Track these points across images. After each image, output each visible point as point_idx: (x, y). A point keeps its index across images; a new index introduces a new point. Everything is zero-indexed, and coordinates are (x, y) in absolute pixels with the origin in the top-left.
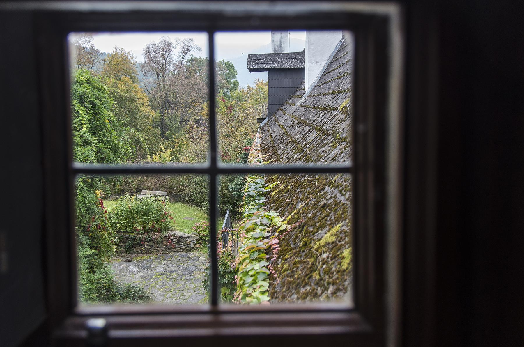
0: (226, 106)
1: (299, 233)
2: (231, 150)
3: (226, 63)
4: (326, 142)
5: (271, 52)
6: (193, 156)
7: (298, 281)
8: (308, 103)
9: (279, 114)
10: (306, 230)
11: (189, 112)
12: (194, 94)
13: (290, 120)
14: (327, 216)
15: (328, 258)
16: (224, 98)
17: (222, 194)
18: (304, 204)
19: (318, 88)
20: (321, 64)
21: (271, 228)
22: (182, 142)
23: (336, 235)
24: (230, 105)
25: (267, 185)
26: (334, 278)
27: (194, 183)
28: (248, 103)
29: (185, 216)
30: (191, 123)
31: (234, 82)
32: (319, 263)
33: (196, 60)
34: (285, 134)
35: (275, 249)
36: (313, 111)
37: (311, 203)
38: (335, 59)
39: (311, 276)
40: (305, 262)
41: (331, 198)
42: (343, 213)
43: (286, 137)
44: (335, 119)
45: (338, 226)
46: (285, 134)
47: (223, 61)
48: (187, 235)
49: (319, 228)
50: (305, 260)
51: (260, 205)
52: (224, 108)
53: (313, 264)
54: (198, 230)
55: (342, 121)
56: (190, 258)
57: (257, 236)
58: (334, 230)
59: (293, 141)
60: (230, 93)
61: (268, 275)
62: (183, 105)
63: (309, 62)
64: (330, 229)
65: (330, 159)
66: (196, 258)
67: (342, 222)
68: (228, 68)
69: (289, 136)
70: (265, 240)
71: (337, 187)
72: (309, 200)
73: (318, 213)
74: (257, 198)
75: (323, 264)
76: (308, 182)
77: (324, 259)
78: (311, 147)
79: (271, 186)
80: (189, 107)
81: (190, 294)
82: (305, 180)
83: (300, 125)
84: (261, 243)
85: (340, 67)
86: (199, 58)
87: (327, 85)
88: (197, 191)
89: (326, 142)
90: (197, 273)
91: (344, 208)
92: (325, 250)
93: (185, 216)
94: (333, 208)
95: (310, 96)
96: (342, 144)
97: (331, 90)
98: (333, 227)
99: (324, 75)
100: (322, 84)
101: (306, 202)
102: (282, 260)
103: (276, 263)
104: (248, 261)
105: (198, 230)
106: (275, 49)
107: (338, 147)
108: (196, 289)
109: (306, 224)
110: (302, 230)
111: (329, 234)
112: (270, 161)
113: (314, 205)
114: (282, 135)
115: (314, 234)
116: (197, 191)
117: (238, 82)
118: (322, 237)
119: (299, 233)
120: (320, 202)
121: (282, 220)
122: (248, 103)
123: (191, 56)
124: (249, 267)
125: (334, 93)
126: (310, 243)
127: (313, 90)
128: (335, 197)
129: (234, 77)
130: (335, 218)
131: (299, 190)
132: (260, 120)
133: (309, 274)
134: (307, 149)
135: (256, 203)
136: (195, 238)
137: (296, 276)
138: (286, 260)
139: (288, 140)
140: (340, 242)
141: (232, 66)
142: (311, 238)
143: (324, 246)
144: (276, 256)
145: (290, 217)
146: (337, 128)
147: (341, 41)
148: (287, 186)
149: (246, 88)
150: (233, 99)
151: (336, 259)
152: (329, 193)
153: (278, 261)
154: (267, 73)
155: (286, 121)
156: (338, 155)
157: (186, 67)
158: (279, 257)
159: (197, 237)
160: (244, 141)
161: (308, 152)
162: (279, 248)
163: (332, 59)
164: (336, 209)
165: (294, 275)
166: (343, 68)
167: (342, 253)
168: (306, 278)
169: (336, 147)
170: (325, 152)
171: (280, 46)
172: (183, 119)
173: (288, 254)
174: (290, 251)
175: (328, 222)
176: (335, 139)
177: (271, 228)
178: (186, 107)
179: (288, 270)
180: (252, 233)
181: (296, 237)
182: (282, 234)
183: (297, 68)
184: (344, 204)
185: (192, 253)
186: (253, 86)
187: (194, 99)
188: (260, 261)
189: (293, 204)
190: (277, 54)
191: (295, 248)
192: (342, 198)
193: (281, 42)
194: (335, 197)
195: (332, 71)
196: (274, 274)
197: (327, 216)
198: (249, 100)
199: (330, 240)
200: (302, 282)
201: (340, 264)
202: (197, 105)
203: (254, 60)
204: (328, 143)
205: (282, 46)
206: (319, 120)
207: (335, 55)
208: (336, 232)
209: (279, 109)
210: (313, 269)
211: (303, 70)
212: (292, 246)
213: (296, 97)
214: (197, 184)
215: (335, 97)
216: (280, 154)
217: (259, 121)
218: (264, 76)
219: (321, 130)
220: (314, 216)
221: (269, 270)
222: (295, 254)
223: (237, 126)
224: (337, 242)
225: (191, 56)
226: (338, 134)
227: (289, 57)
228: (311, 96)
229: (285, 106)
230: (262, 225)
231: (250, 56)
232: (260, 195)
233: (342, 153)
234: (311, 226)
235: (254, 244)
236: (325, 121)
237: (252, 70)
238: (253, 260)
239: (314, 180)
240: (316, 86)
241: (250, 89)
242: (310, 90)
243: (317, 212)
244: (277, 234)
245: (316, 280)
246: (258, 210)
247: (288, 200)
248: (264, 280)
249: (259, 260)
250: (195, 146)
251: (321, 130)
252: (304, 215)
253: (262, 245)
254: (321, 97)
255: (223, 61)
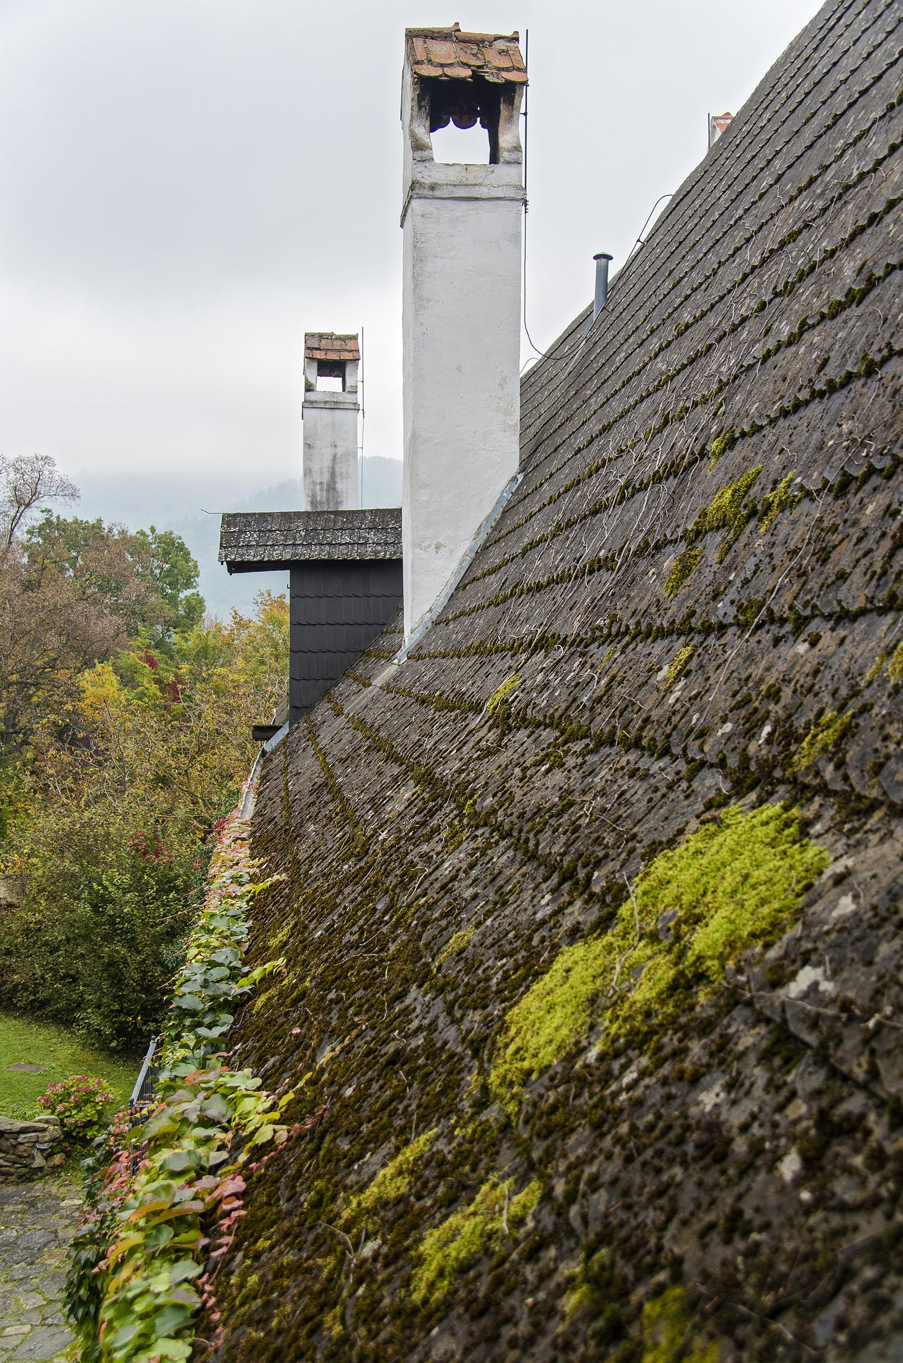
0: (158, 681)
1: (311, 1157)
2: (172, 829)
3: (160, 537)
4: (434, 822)
5: (303, 506)
6: (43, 851)
7: (279, 1341)
8: (405, 683)
9: (323, 711)
10: (329, 1150)
11: (35, 699)
12: (53, 640)
13: (348, 737)
14: (398, 1097)
15: (376, 1257)
16: (155, 653)
17: (143, 979)
18: (338, 1049)
19: (442, 630)
20: (452, 552)
21: (230, 1135)
22: (11, 803)
23: (412, 1172)
24: (172, 678)
25: (246, 969)
26: (383, 1335)
27: (46, 944)
28: (233, 673)
29: (16, 1059)
30: (42, 737)
31: (187, 599)
32: (347, 1277)
33: (61, 526)
34: (328, 787)
35: (227, 1214)
36: (416, 707)
37: (361, 1047)
38: (496, 535)
39: (318, 1326)
40: (308, 1270)
41: (420, 1028)
42: (443, 1092)
43: (327, 798)
44: (471, 744)
45: (423, 1138)
46: (328, 787)
47: (153, 530)
48: (20, 1124)
49: (368, 1142)
50: (311, 1262)
51: (214, 1046)
52: (154, 688)
53: (330, 1280)
54: (60, 1108)
55: (489, 753)
56: (32, 1204)
57: (178, 1167)
58: (409, 1154)
59: (347, 815)
60: (175, 638)
61: (196, 1314)
62: (14, 678)
63: (414, 545)
64: (398, 1149)
65: (437, 885)
66: (50, 1202)
67: (438, 1121)
68: (166, 553)
69: (337, 792)
70: (207, 1181)
71: (441, 990)
72: (354, 1033)
73: (375, 1086)
74: (207, 1020)
75: (359, 1282)
76: (363, 966)
77: (364, 1261)
78: (391, 840)
79: (257, 974)
80: (37, 685)
81: (27, 1328)
82: (355, 959)
83: (375, 756)
84: (189, 1193)
85: (505, 563)
86: (70, 520)
87: (467, 621)
88: (54, 971)
89: (434, 822)
90: (51, 1256)
91: (451, 1073)
92: (370, 1227)
93: (16, 1059)
94: (420, 1068)
95: (416, 655)
96: (479, 832)
97: (474, 640)
98: (407, 1142)
99: (461, 587)
100: (455, 618)
101: (347, 1042)
102: (245, 1257)
103: (224, 1268)
104: (139, 1258)
105: (60, 1108)
106: (314, 496)
107: (465, 844)
108: (48, 1311)
109: (333, 1124)
110: (318, 1149)
111: (389, 1170)
112: (269, 882)
113: (367, 1054)
114: (317, 790)
115: (349, 1165)
116: (54, 971)
117: (201, 601)
118: (372, 1178)
119: (311, 1157)
120: (385, 1042)
121: (268, 1105)
122: (233, 673)
123: (45, 515)
124: (137, 1284)
125: (479, 650)
126: (334, 1198)
127: (427, 636)
128: (432, 1027)
129: (188, 585)
130: (419, 1106)
131: (332, 995)
132: (263, 732)
133: (312, 1317)
134: (377, 847)
135: (199, 1039)
136: (47, 1136)
137: (274, 1323)
138: (257, 1257)
139: (331, 807)
140: (419, 1198)
141: (181, 547)
142: (336, 1178)
143: (371, 1212)
144: (229, 1239)
145: (290, 1096)
146: (472, 775)
147: (514, 479)
148: (302, 979)
149: (227, 621)
150: (185, 657)
151: (401, 1262)
152: (418, 1011)
153: (232, 1259)
154: (284, 576)
155: (337, 739)
156: (462, 875)
157: (26, 548)
158: (236, 1247)
159: (53, 1131)
160: (215, 799)
161: (379, 858)
162: (243, 1213)
163: (489, 535)
164: (428, 1075)
165: (270, 1317)
166: (512, 567)
167: (420, 1240)
168: (304, 1332)
169: (460, 843)
170: (426, 857)
171: (331, 487)
172: (14, 725)
173: (266, 1234)
174: (274, 1222)
175: (399, 1122)
176: (461, 816)
177: (230, 1135)
178: (23, 685)
179: (255, 1298)
180: (165, 1154)
181: (299, 1173)
182: (258, 1160)
183: (383, 561)
184: (452, 1055)
185: (39, 1185)
186: (251, 613)
187: (53, 655)
188: (177, 1260)
189: (307, 1047)
190: (320, 513)
191: (290, 1213)
192: (451, 1033)
193: (333, 475)
194: (432, 1027)
195: (484, 575)
196: (212, 1310)
197: (398, 1097)
198: (240, 662)
199: (391, 1192)
200: (290, 1346)
201: (407, 1282)
202: (61, 675)
203: (241, 532)
204: (437, 830)
205: (339, 486)
206: (429, 744)
207: (498, 524)
208: (416, 1160)
209: (326, 694)
210: (326, 1298)
211: (395, 566)
212: (284, 1206)
213: (379, 658)
214: (58, 949)
215: (483, 664)
216: (302, 856)
217: (258, 734)
218: (278, 583)
219: (427, 779)
220: (362, 1095)
221: (200, 1292)
222: (286, 1235)
223: (193, 748)
224: (412, 1199)
225: (45, 515)
226: (471, 796)
227: (357, 524)
228: (420, 658)
229: (342, 687)
230: (206, 1122)
231: (229, 520)
232: (220, 1005)
233: (472, 866)
234: (347, 1133)
235: (163, 1195)
236: (442, 747)
237: (236, 567)
238: (153, 1257)
239: (382, 960)
240: (436, 623)
241: (241, 624)
242: (417, 636)
243: (371, 1080)
244: (243, 1157)
245: (330, 1339)
246: (203, 1065)
247: (296, 1031)
248: (177, 1335)
249: (174, 1254)
250: (52, 818)
251: (427, 779)
252: (334, 1088)
253: (185, 1197)
254: (446, 662)
255: (153, 530)
